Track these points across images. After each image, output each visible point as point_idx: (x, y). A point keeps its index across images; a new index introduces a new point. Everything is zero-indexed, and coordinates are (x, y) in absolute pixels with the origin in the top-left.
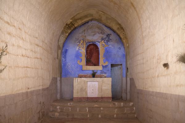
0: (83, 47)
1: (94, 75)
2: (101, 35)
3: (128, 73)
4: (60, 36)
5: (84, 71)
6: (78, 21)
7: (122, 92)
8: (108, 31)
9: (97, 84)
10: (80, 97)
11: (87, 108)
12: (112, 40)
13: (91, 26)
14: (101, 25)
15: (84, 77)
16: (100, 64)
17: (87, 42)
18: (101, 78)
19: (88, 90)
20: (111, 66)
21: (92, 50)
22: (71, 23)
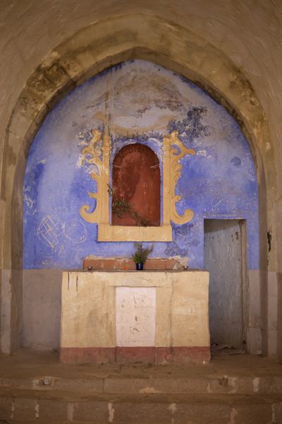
0: (101, 157)
1: (140, 262)
2: (167, 112)
3: (269, 254)
4: (13, 112)
5: (106, 247)
6: (80, 57)
7: (244, 325)
8: (194, 98)
9: (154, 297)
10: (85, 345)
11: (110, 405)
12: (210, 130)
13: (130, 78)
14: (166, 74)
15: (102, 266)
16: (165, 219)
17: (114, 138)
18: (169, 274)
19: (118, 318)
20: (205, 223)
21: (136, 170)
22: (56, 63)
